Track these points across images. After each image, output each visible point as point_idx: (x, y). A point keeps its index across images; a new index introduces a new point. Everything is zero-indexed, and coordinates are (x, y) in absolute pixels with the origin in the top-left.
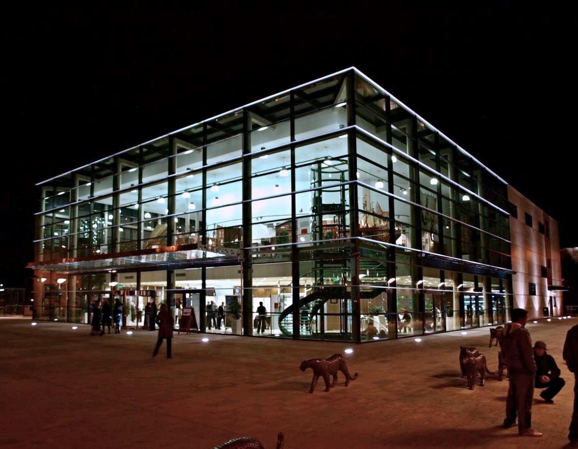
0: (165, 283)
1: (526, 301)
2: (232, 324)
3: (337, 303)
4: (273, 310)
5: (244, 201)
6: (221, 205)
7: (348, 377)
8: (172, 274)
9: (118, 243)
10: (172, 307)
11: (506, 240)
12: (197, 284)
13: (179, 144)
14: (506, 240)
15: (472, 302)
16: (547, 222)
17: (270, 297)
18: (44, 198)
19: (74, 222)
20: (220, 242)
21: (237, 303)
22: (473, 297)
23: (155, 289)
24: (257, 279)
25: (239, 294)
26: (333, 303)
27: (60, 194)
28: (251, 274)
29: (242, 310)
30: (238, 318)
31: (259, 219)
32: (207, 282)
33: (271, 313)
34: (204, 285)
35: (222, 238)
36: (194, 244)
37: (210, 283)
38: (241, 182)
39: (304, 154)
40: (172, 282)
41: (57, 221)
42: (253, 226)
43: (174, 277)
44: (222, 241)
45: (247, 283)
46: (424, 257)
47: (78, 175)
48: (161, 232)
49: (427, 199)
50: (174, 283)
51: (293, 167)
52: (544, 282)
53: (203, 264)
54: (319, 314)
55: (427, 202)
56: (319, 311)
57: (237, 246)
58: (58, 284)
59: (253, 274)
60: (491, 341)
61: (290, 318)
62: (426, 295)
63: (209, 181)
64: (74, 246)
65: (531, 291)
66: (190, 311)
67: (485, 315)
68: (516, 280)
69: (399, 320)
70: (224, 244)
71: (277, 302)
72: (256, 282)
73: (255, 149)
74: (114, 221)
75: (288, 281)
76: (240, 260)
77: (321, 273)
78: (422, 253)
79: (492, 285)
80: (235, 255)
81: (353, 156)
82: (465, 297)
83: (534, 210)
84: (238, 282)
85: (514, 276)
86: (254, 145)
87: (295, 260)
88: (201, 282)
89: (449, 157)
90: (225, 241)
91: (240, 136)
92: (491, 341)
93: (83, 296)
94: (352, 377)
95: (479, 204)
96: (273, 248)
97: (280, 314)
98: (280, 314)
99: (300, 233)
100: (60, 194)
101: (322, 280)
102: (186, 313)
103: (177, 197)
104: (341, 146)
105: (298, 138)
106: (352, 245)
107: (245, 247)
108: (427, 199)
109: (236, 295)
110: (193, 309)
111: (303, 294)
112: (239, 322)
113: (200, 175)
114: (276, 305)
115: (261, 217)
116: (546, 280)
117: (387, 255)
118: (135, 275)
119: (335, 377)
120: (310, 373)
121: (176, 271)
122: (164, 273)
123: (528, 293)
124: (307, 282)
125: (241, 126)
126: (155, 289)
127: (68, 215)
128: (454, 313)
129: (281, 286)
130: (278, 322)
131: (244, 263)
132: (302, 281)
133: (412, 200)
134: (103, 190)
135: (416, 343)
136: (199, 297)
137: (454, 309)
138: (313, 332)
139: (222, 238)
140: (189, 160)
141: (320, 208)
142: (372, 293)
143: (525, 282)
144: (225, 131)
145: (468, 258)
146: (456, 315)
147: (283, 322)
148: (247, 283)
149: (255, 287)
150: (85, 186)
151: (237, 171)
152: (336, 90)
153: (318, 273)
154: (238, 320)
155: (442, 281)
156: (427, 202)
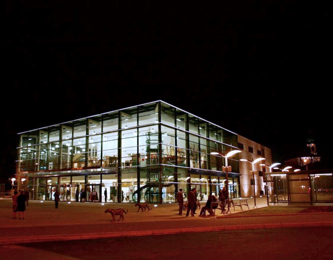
0: (84, 181)
1: (249, 188)
2: (113, 199)
4: (130, 192)
5: (119, 130)
6: (109, 149)
8: (87, 178)
10: (87, 192)
11: (236, 160)
12: (98, 182)
13: (90, 121)
14: (236, 160)
16: (263, 150)
17: (129, 187)
20: (107, 163)
22: (232, 186)
23: (79, 184)
24: (123, 179)
25: (116, 186)
28: (121, 186)
29: (117, 192)
30: (115, 195)
33: (129, 193)
34: (101, 181)
40: (87, 181)
41: (25, 150)
42: (122, 140)
43: (88, 179)
45: (119, 181)
46: (191, 170)
47: (40, 131)
48: (79, 157)
50: (88, 181)
51: (138, 136)
52: (261, 179)
53: (101, 173)
54: (148, 193)
56: (148, 192)
57: (115, 165)
58: (22, 181)
59: (122, 177)
61: (136, 195)
62: (191, 185)
63: (104, 139)
65: (252, 182)
66: (95, 193)
68: (242, 178)
72: (123, 180)
74: (60, 154)
75: (136, 180)
76: (117, 172)
77: (149, 177)
78: (190, 169)
80: (115, 170)
81: (160, 134)
83: (253, 144)
84: (116, 180)
85: (240, 176)
86: (123, 123)
87: (139, 172)
88: (100, 180)
89: (205, 127)
91: (117, 119)
93: (23, 188)
94: (150, 209)
96: (131, 165)
101: (149, 179)
104: (155, 129)
106: (159, 167)
107: (119, 166)
109: (114, 186)
110: (96, 192)
111: (141, 186)
113: (101, 135)
114: (131, 190)
116: (262, 178)
117: (175, 169)
118: (69, 178)
119: (145, 209)
121: (89, 176)
122: (84, 177)
123: (250, 184)
124: (144, 181)
125: (118, 116)
126: (79, 184)
129: (134, 182)
131: (118, 173)
132: (141, 180)
133: (186, 148)
134: (54, 138)
136: (99, 187)
140: (95, 129)
141: (149, 150)
142: (168, 185)
143: (248, 179)
144: (112, 117)
145: (216, 169)
148: (119, 181)
149: (123, 182)
151: (116, 135)
153: (148, 177)
155: (200, 178)
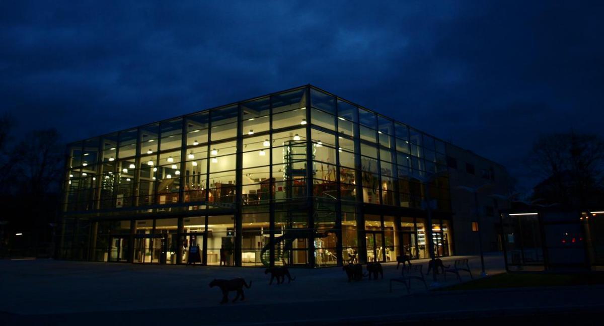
3: (303, 241)
9: (137, 196)
15: (438, 238)
19: (99, 178)
21: (230, 242)
27: (87, 154)
36: (147, 165)
37: (210, 226)
38: (235, 156)
39: (280, 139)
49: (370, 163)
51: (271, 165)
60: (429, 270)
64: (98, 197)
66: (196, 249)
69: (283, 244)
71: (259, 241)
73: (247, 131)
79: (143, 262)
92: (429, 270)
97: (261, 250)
98: (261, 250)
100: (87, 154)
105: (275, 127)
109: (229, 236)
112: (232, 257)
128: (395, 248)
130: (259, 256)
135: (150, 213)
138: (285, 263)
152: (301, 95)
153: (290, 219)
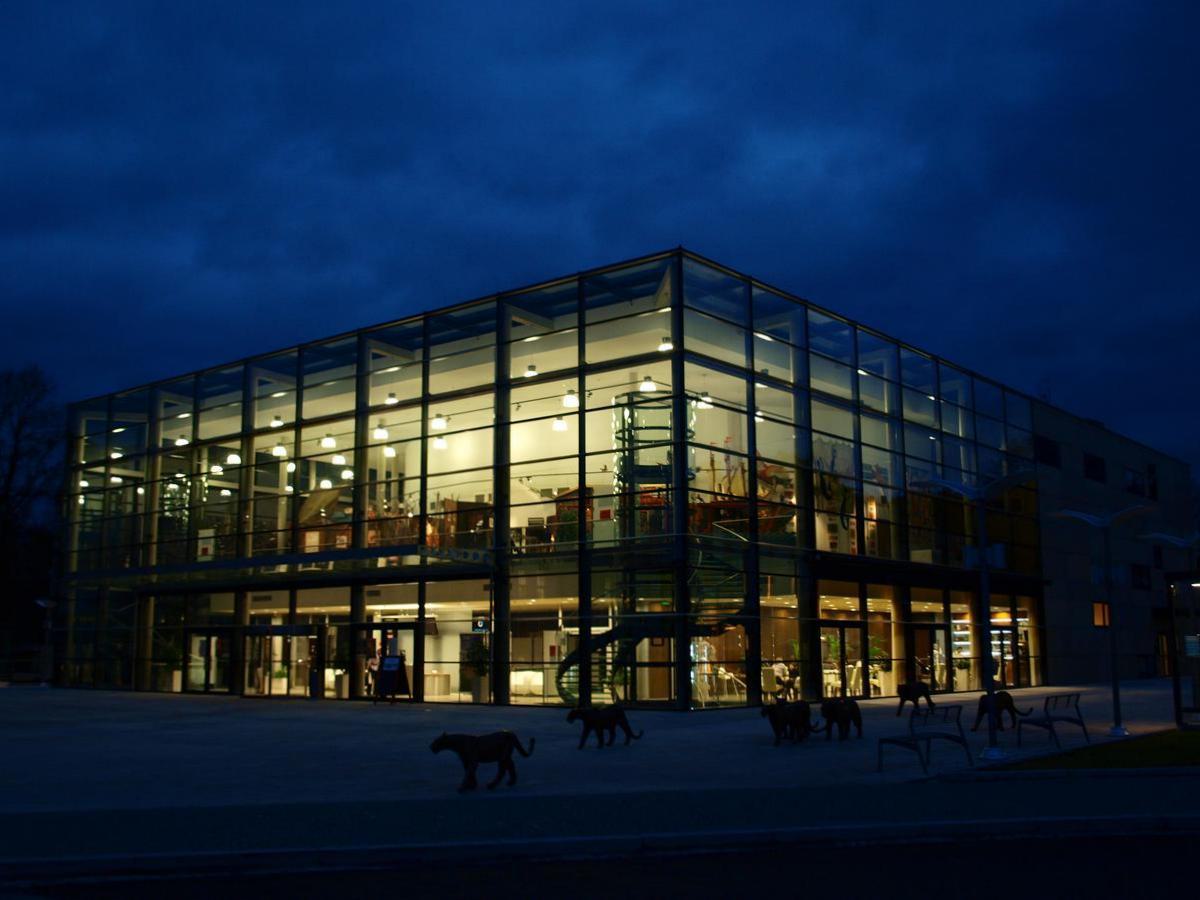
3: (663, 645)
7: (629, 734)
12: (407, 610)
18: (82, 437)
20: (449, 530)
26: (656, 645)
27: (116, 431)
31: (525, 480)
32: (646, 669)
35: (452, 523)
39: (605, 387)
43: (362, 598)
44: (453, 529)
49: (834, 451)
53: (421, 575)
55: (834, 457)
63: (436, 425)
66: (397, 661)
67: (972, 669)
70: (456, 535)
71: (553, 644)
73: (519, 368)
82: (993, 632)
90: (458, 528)
95: (961, 448)
97: (557, 666)
98: (557, 666)
99: (599, 518)
101: (633, 604)
102: (389, 666)
103: (370, 450)
108: (834, 451)
109: (477, 632)
112: (485, 681)
115: (528, 478)
119: (613, 734)
120: (579, 723)
121: (367, 588)
122: (346, 591)
127: (651, 695)
134: (221, 425)
137: (894, 657)
139: (452, 523)
141: (631, 471)
146: (898, 667)
147: (564, 680)
150: (215, 447)
153: (628, 591)
154: (482, 678)
156: (834, 457)
